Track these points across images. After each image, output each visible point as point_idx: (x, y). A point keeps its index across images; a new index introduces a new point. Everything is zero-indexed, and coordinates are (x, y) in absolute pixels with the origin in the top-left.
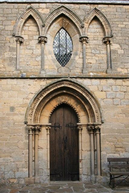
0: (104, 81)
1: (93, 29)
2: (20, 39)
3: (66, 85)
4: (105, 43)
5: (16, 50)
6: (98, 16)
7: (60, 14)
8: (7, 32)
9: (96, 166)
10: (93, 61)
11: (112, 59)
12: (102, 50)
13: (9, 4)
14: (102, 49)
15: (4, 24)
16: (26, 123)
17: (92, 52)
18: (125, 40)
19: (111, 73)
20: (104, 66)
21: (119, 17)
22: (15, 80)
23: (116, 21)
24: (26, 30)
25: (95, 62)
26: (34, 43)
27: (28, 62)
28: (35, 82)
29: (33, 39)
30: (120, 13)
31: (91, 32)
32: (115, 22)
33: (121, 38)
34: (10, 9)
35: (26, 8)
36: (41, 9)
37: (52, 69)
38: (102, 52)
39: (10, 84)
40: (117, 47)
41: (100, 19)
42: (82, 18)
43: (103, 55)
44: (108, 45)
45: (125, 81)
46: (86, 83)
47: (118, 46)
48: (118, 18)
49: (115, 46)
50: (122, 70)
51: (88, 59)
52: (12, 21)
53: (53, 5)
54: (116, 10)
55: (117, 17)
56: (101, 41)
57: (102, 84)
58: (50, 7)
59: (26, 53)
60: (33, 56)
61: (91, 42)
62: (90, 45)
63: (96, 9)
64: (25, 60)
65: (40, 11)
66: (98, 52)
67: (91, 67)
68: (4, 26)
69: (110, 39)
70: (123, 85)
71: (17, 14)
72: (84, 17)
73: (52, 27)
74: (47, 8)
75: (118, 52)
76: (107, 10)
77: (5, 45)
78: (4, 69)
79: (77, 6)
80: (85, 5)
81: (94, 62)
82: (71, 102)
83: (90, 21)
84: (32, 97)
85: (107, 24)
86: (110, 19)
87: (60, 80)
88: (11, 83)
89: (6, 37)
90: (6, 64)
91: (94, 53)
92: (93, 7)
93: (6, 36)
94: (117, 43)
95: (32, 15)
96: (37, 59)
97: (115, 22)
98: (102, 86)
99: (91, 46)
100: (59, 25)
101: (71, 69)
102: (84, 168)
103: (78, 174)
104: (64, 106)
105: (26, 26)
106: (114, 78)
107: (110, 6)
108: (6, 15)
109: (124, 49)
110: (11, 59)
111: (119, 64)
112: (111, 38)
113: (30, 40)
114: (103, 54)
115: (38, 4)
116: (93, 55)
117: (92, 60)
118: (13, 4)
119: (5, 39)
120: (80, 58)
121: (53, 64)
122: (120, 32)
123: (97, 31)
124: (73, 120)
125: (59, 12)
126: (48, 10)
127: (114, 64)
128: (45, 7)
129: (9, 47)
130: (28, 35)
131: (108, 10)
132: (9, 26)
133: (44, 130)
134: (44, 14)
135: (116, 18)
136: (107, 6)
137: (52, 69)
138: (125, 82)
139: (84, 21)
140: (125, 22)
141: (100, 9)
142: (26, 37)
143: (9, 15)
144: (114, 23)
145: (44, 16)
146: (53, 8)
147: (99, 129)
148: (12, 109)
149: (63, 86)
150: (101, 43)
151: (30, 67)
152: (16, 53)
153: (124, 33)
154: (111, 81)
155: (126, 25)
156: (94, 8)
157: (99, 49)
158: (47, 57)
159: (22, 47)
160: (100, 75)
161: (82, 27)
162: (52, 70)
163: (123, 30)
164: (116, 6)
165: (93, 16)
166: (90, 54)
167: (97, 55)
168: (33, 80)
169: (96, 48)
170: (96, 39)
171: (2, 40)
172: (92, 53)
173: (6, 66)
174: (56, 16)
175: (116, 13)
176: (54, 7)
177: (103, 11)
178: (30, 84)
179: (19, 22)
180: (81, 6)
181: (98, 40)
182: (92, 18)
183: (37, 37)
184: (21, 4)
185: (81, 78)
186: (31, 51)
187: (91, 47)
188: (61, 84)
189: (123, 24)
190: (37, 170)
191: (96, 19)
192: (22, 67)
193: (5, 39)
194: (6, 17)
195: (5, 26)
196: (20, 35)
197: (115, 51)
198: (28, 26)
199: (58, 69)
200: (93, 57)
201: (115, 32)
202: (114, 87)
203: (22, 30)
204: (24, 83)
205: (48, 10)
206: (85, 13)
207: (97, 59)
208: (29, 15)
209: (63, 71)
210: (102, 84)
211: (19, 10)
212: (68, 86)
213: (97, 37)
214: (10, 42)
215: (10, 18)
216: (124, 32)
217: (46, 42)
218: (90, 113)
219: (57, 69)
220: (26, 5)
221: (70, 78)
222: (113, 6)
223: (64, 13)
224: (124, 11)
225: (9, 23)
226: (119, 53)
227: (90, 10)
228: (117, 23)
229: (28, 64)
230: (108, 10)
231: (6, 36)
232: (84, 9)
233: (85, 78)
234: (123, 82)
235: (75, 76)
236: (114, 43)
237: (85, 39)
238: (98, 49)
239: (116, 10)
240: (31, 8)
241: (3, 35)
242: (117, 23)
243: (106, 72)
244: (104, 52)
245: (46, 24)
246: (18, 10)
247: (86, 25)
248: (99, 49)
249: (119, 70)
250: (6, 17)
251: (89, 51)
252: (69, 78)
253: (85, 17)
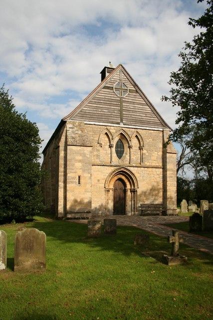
4: (140, 149)
5: (98, 150)
9: (134, 208)
10: (134, 158)
16: (105, 188)
26: (107, 147)
42: (130, 136)
46: (131, 169)
49: (144, 151)
65: (111, 130)
82: (123, 178)
84: (107, 175)
92: (135, 130)
102: (128, 208)
103: (117, 214)
104: (120, 179)
124: (123, 187)
133: (111, 191)
147: (137, 191)
148: (99, 180)
160: (137, 165)
161: (130, 141)
177: (140, 132)
197: (145, 154)
202: (144, 172)
218: (132, 182)
225: (96, 136)
230: (143, 132)
243: (140, 164)
244: (139, 153)
249: (146, 163)
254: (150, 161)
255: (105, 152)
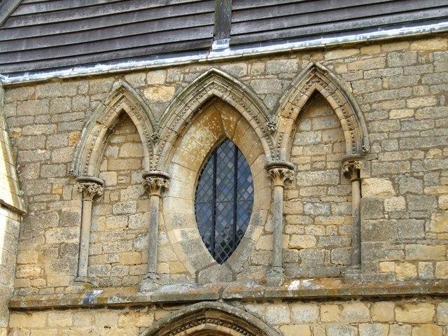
0: (330, 310)
1: (312, 135)
2: (93, 188)
3: (212, 326)
4: (347, 175)
6: (323, 91)
7: (205, 97)
8: (56, 168)
10: (306, 242)
11: (363, 232)
12: (337, 203)
13: (65, 84)
14: (338, 200)
15: (50, 144)
17: (306, 210)
18: (411, 160)
19: (359, 278)
20: (340, 256)
21: (395, 86)
22: (69, 314)
23: (381, 98)
24: (112, 156)
25: (312, 244)
27: (111, 255)
28: (122, 317)
29: (130, 184)
30: (398, 71)
31: (306, 146)
32: (380, 102)
33: (397, 156)
34: (67, 99)
35: (111, 90)
36: (151, 89)
37: (180, 273)
38: (336, 209)
39: (54, 327)
40: (381, 191)
41: (330, 99)
43: (337, 221)
44: (356, 185)
45: (406, 305)
47: (386, 185)
48: (389, 89)
49: (375, 187)
50: (398, 269)
51: (291, 235)
52: (71, 135)
53: (186, 73)
54: (386, 61)
55: (386, 85)
56: (336, 172)
57: (325, 317)
58: (177, 78)
59: (109, 226)
60: (129, 237)
61: (307, 179)
62: (298, 188)
63: (314, 68)
64: (105, 247)
66: (324, 209)
67: (300, 261)
68: (49, 152)
69: (360, 164)
70: (395, 322)
71: (85, 111)
72: (275, 98)
73: (186, 139)
74: (168, 84)
75: (385, 204)
76: (353, 66)
77: (48, 208)
78: (40, 282)
79: (259, 66)
80: (283, 61)
81: (310, 246)
83: (297, 111)
85: (175, 115)
86: (363, 95)
87: (192, 308)
88: (59, 322)
89: (52, 184)
90: (48, 265)
91: (309, 215)
93: (52, 180)
94: (381, 176)
95: (127, 110)
96: (138, 245)
97: (380, 102)
98: (324, 326)
99: (303, 193)
100: (208, 131)
101: (237, 270)
105: (112, 145)
106: (365, 299)
107: (364, 50)
108: (55, 119)
109: (405, 196)
110: (63, 249)
111: (385, 245)
112: (360, 162)
113: (121, 186)
114: (341, 214)
115: (143, 76)
116: (307, 220)
117: (304, 240)
118: (77, 83)
119: (49, 191)
120: (265, 233)
121: (183, 256)
122: (396, 135)
123: (325, 139)
125: (204, 92)
126: (172, 90)
127: (370, 247)
128: (162, 82)
129: (60, 212)
130: (117, 171)
131: (358, 64)
132: (63, 151)
134: (159, 103)
135: (384, 89)
136: (355, 52)
137: (180, 273)
138: (403, 309)
139: (274, 112)
140: (413, 100)
141: (331, 64)
142: (111, 179)
143: (66, 117)
144: (374, 106)
145: (157, 109)
146: (184, 81)
149: (202, 327)
150: (336, 179)
151: (117, 269)
152: (78, 229)
153: (410, 137)
154: (356, 309)
155: (416, 110)
156: (311, 64)
157: (328, 199)
158: (168, 237)
159: (98, 210)
162: (178, 275)
163: (406, 126)
164: (386, 48)
165: (309, 93)
166: (299, 219)
167: (321, 218)
168: (119, 311)
169: (318, 197)
170: (319, 165)
171: (43, 194)
172: (303, 214)
173: (48, 272)
174: (194, 106)
175: (385, 72)
176: (188, 78)
178: (110, 324)
179: (91, 136)
180: (270, 63)
181: (325, 169)
182: (305, 98)
183: (137, 177)
184: (98, 81)
185: (260, 301)
186: (122, 222)
187: (301, 194)
188: (197, 322)
189: (406, 107)
190: (433, 292)
191: (316, 99)
192: (97, 272)
193: (49, 191)
194: (56, 123)
195: (52, 149)
196: (91, 173)
197: (374, 205)
198: (119, 145)
199: (197, 273)
200: (309, 229)
201: (378, 137)
203: (103, 157)
204: (93, 322)
205: (172, 90)
206: (282, 85)
207: (320, 231)
208: (118, 109)
209: (215, 280)
210: (325, 317)
211: (93, 98)
212: (219, 328)
213: (323, 158)
214: (62, 199)
215: (66, 126)
216: (407, 134)
217: (164, 189)
219: (192, 271)
220: (109, 81)
221: (226, 300)
222: (376, 49)
223: (219, 94)
224: (414, 61)
225: (63, 140)
226: (388, 208)
227: (297, 73)
228: (386, 105)
229: (112, 260)
231: (52, 180)
232: (277, 74)
233: (271, 301)
234: (399, 312)
235: (237, 296)
236: (372, 177)
237: (276, 170)
238: (323, 199)
239: (386, 61)
240: (122, 89)
241: (46, 178)
242: (386, 105)
245: (162, 133)
246: (88, 98)
247: (283, 125)
248: (328, 199)
249: (387, 267)
250: (56, 123)
251: (297, 207)
252: (221, 301)
253: (279, 98)
254: (420, 250)
255: (116, 224)
